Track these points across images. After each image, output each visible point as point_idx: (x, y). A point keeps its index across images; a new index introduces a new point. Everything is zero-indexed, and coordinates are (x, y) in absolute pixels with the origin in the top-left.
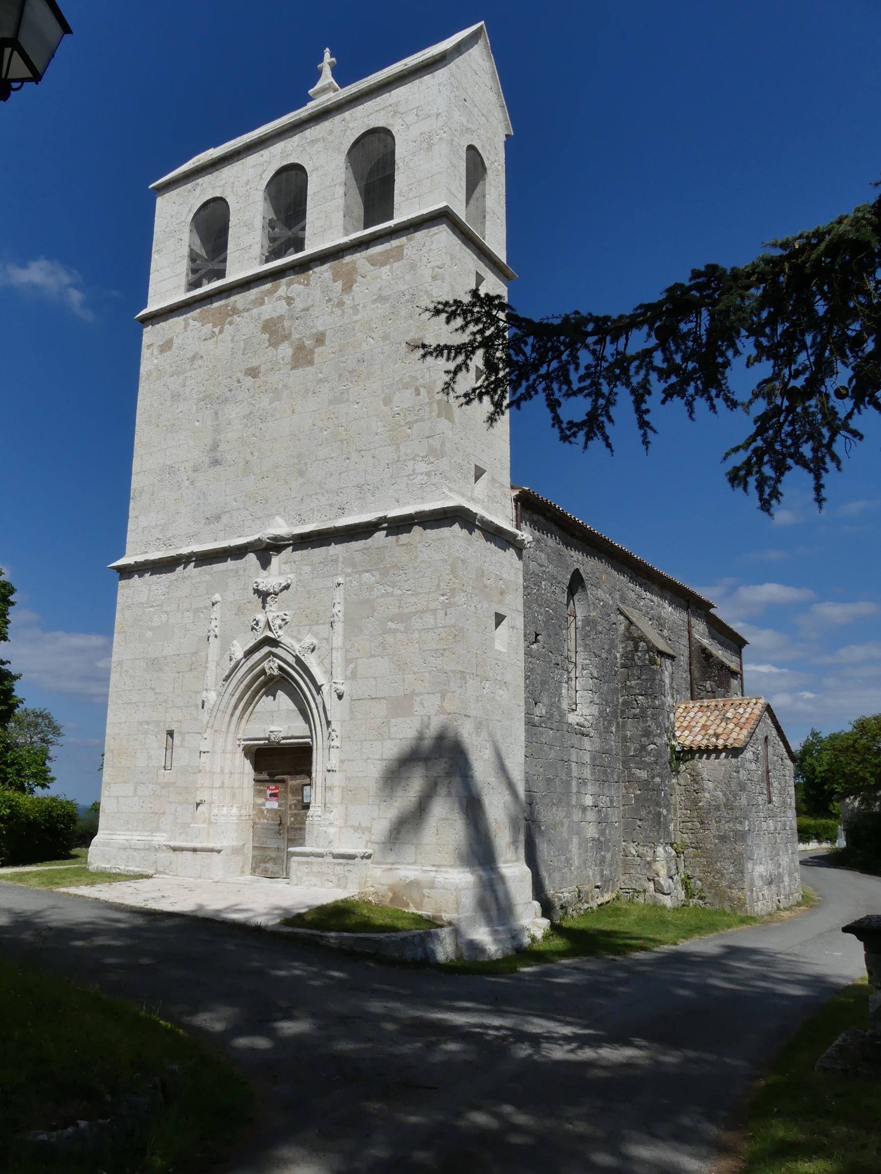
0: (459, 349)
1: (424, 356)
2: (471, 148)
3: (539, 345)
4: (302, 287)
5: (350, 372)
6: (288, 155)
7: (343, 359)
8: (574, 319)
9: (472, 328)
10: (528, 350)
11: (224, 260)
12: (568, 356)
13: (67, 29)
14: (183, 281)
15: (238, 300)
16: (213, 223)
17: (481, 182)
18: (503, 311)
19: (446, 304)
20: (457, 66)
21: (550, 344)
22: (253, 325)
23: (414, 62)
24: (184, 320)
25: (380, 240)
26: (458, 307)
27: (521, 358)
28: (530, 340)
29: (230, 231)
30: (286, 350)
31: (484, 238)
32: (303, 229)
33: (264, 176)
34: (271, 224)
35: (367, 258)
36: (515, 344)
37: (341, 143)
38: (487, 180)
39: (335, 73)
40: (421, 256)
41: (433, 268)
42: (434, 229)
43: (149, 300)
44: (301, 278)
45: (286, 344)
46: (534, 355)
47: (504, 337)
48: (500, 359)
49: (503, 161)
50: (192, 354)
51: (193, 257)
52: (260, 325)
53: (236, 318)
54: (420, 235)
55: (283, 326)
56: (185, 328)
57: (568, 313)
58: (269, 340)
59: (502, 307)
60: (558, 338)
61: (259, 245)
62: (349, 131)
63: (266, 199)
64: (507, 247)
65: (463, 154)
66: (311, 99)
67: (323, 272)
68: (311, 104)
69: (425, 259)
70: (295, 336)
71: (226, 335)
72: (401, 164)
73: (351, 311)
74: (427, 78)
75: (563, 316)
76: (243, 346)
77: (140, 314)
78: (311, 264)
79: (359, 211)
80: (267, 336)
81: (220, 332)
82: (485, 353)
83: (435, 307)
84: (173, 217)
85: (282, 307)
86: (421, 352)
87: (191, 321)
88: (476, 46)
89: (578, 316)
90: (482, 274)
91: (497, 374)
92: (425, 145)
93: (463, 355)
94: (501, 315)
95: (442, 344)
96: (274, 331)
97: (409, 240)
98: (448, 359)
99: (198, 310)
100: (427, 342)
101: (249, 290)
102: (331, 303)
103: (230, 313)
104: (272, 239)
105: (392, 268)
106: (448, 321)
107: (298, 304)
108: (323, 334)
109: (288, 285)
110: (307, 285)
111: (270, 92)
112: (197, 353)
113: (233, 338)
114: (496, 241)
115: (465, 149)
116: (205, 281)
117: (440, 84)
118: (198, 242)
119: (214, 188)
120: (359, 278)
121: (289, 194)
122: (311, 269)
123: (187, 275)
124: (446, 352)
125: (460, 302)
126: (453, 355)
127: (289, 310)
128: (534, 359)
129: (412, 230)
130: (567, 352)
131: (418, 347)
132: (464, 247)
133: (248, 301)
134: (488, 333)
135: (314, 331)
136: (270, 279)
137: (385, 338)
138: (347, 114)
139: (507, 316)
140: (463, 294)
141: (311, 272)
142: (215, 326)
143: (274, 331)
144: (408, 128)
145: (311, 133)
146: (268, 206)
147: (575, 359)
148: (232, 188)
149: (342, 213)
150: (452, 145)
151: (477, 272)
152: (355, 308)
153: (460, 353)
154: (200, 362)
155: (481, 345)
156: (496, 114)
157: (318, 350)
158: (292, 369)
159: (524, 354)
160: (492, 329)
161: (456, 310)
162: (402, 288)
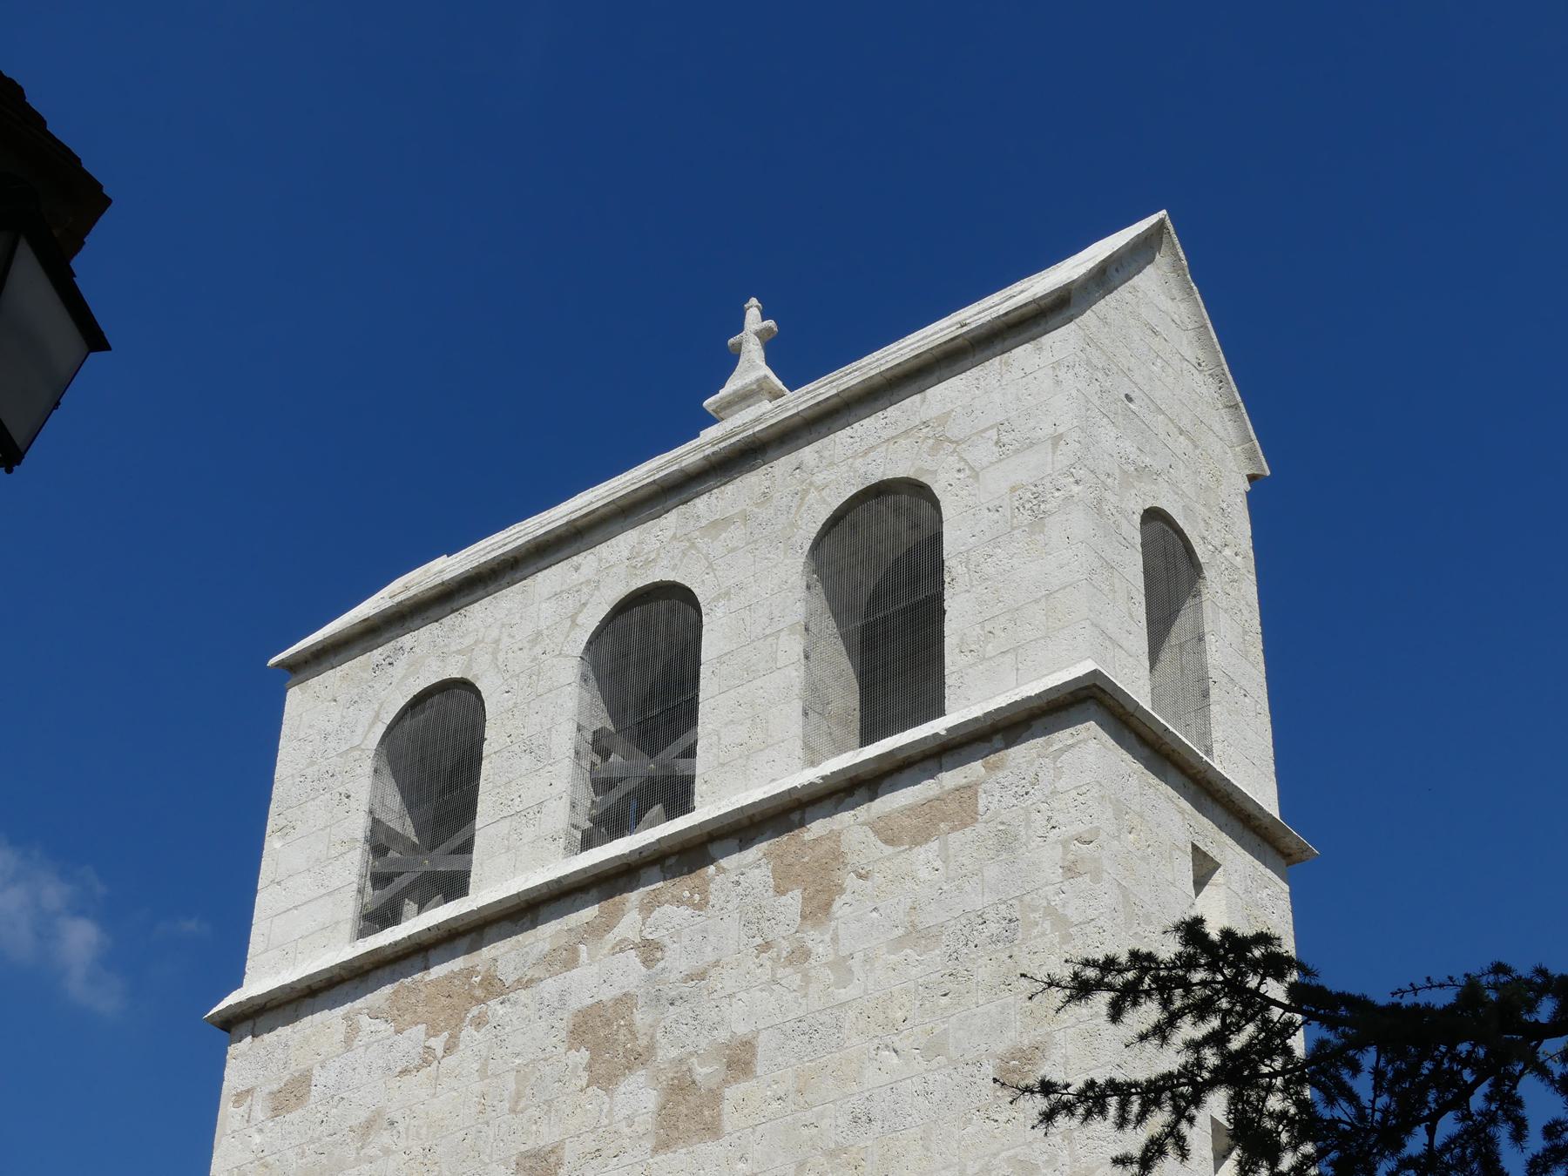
0: (1153, 1092)
1: (1048, 1117)
2: (1154, 517)
3: (1397, 1072)
4: (685, 912)
5: (831, 1154)
6: (647, 562)
7: (809, 1116)
8: (1495, 987)
9: (1189, 1030)
10: (1363, 1086)
11: (467, 847)
12: (1489, 1098)
13: (95, 340)
14: (348, 910)
15: (502, 955)
16: (438, 754)
17: (1190, 602)
18: (1279, 977)
19: (1109, 965)
20: (1104, 321)
21: (1428, 1066)
22: (543, 1025)
23: (986, 317)
24: (346, 1018)
25: (907, 774)
26: (1144, 971)
27: (1342, 1112)
28: (1369, 1058)
29: (486, 768)
30: (639, 1096)
31: (1209, 752)
32: (690, 753)
33: (580, 619)
34: (600, 745)
35: (871, 825)
36: (1324, 1067)
37: (793, 525)
38: (1206, 595)
39: (775, 353)
40: (1027, 811)
41: (1065, 844)
42: (1063, 737)
43: (249, 964)
44: (683, 886)
45: (639, 1077)
46: (1383, 1101)
47: (1288, 1052)
48: (1282, 1116)
49: (1246, 544)
50: (363, 1115)
51: (379, 842)
52: (563, 1027)
53: (495, 1008)
54: (1022, 754)
55: (630, 1026)
56: (348, 1042)
57: (1475, 971)
58: (589, 1068)
59: (1276, 965)
60: (1452, 1047)
61: (566, 802)
62: (813, 495)
63: (584, 679)
64: (1278, 774)
65: (1133, 532)
66: (710, 420)
67: (747, 867)
68: (709, 434)
69: (1039, 820)
70: (667, 1052)
71: (465, 1059)
72: (961, 569)
73: (829, 975)
74: (1023, 355)
75: (1462, 981)
76: (512, 1086)
77: (215, 1010)
78: (713, 849)
79: (846, 697)
80: (583, 1056)
81: (448, 1050)
82: (1233, 1101)
83: (1076, 976)
84: (330, 739)
85: (629, 972)
86: (1041, 1103)
87: (364, 1020)
88: (1149, 270)
89: (1503, 979)
90: (1213, 852)
91: (1274, 1161)
92: (1025, 517)
93: (1167, 1107)
94: (1275, 990)
95: (1100, 1081)
96: (604, 1040)
97: (991, 769)
98: (1122, 1123)
99: (387, 990)
100: (1057, 1077)
101: (534, 925)
102: (773, 953)
103: (479, 993)
104: (602, 785)
105: (945, 847)
106: (1116, 1013)
107: (676, 961)
108: (748, 1045)
109: (647, 908)
110: (699, 907)
111: (601, 402)
112: (379, 1113)
113: (485, 1065)
114: (1246, 757)
115: (1137, 519)
116: (410, 906)
117: (1056, 365)
118: (394, 800)
119: (443, 657)
120: (851, 881)
121: (650, 666)
122: (712, 861)
123: (360, 891)
124: (1113, 1102)
125: (1150, 957)
126: (1135, 1108)
127: (649, 978)
128: (1385, 1111)
129: (998, 740)
130: (1484, 1088)
131: (1028, 1090)
132: (1152, 779)
133: (531, 960)
134: (1236, 1043)
135: (722, 1035)
136: (594, 893)
137: (933, 1048)
138: (807, 454)
139: (1293, 990)
140: (1158, 936)
141: (712, 869)
142: (433, 1032)
143: (604, 1040)
144: (976, 476)
145: (709, 504)
146: (592, 696)
147: (1509, 1106)
148: (495, 654)
149: (797, 706)
150: (1100, 512)
151: (1195, 848)
152: (842, 966)
153: (1158, 1103)
154: (386, 1138)
155: (1221, 1077)
156: (1217, 427)
157: (732, 1093)
158: (655, 1151)
159: (1352, 1098)
160: (1250, 1029)
161: (1140, 980)
162: (977, 901)
